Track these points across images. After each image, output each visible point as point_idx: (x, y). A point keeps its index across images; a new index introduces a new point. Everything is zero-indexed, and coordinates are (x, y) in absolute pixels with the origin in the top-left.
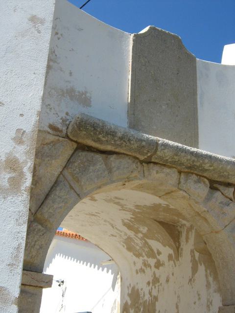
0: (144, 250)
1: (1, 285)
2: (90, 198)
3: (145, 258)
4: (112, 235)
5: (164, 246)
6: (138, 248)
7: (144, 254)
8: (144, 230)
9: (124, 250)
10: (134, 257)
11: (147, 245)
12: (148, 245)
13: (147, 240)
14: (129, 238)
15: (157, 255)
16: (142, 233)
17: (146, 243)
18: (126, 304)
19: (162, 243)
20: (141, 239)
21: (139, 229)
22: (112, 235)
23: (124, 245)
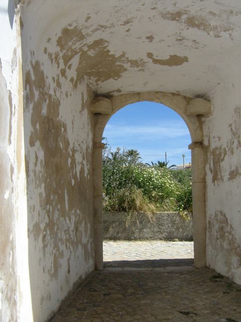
0: (68, 50)
1: (7, 320)
2: (57, 255)
3: (61, 55)
4: (88, 18)
5: (77, 71)
6: (70, 44)
7: (64, 51)
8: (91, 53)
9: (64, 24)
10: (57, 38)
11: (74, 53)
12: (75, 54)
13: (79, 54)
14: (82, 37)
15: (67, 66)
16: (87, 51)
17: (76, 53)
18: (27, 95)
19: (78, 68)
20: (81, 49)
21: (92, 50)
22: (88, 18)
23: (72, 27)
